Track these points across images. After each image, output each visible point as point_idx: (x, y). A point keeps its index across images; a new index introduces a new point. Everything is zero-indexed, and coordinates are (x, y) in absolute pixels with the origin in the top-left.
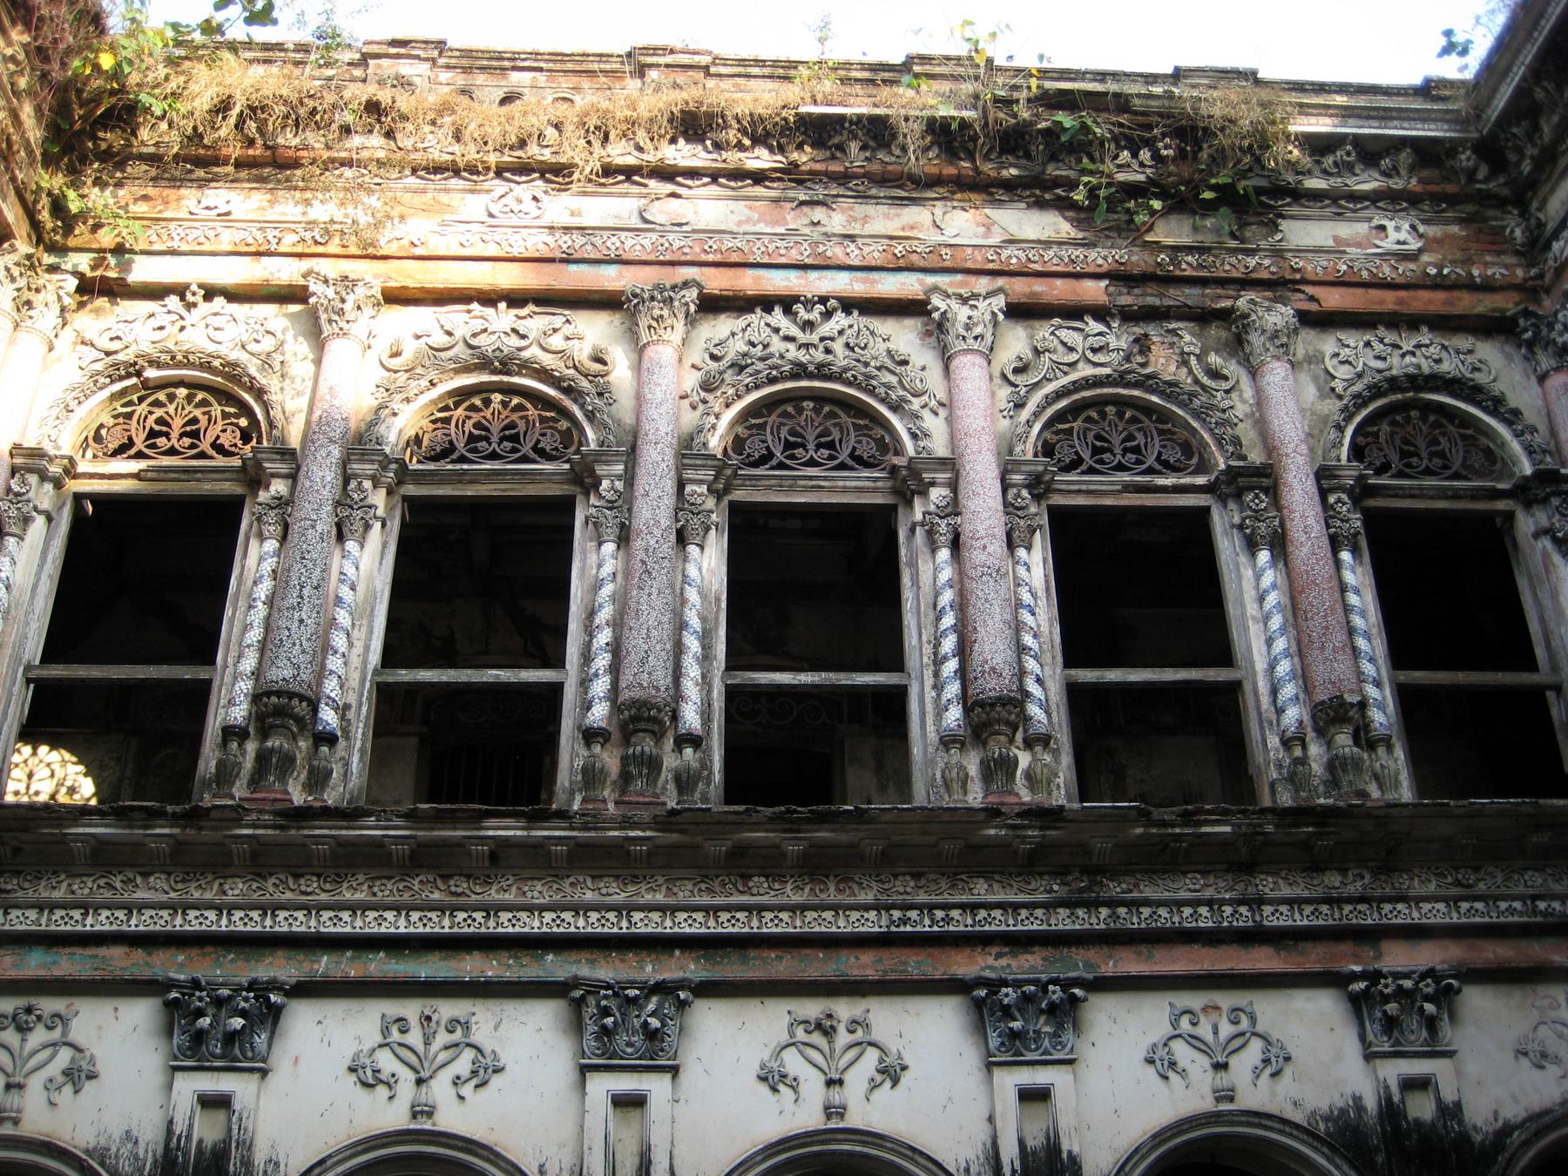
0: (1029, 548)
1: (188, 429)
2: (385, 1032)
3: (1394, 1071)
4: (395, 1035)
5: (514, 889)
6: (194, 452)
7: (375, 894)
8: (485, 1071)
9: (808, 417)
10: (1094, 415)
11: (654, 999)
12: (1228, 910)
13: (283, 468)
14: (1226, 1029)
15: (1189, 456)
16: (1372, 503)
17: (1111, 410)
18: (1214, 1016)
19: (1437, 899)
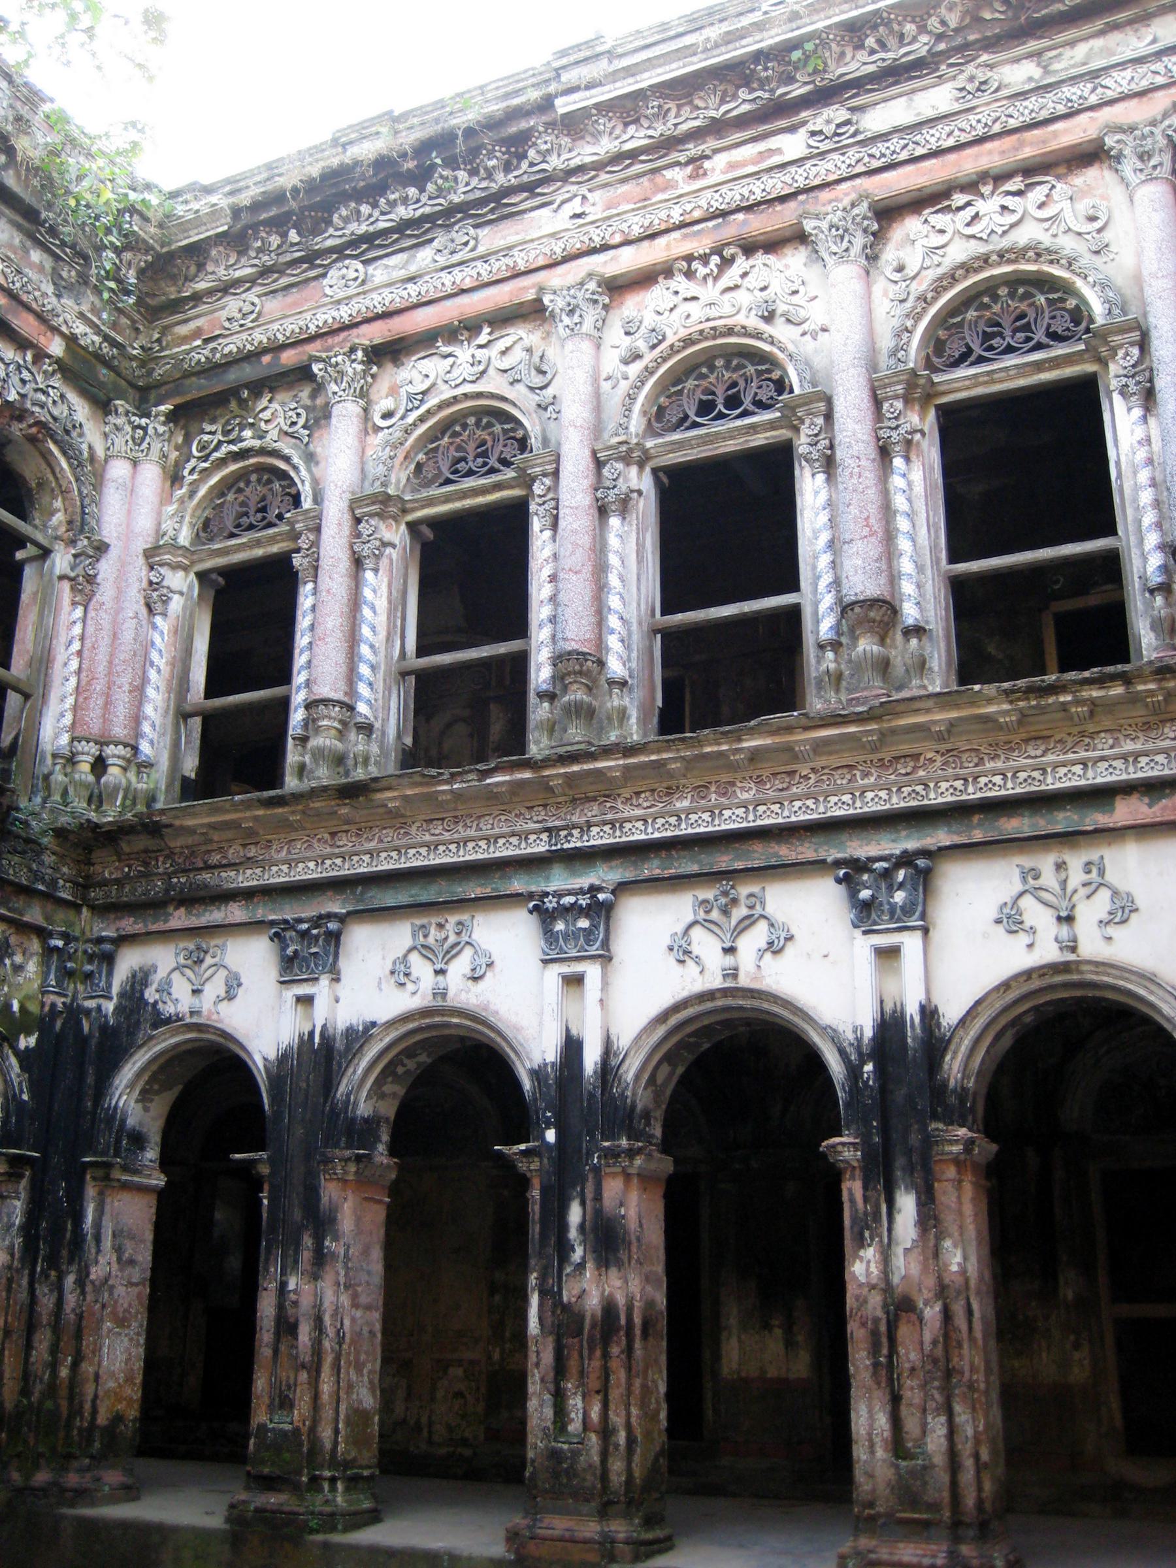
0: (376, 571)
1: (730, 392)
2: (1024, 880)
6: (265, 522)
9: (1005, 306)
15: (1077, 323)
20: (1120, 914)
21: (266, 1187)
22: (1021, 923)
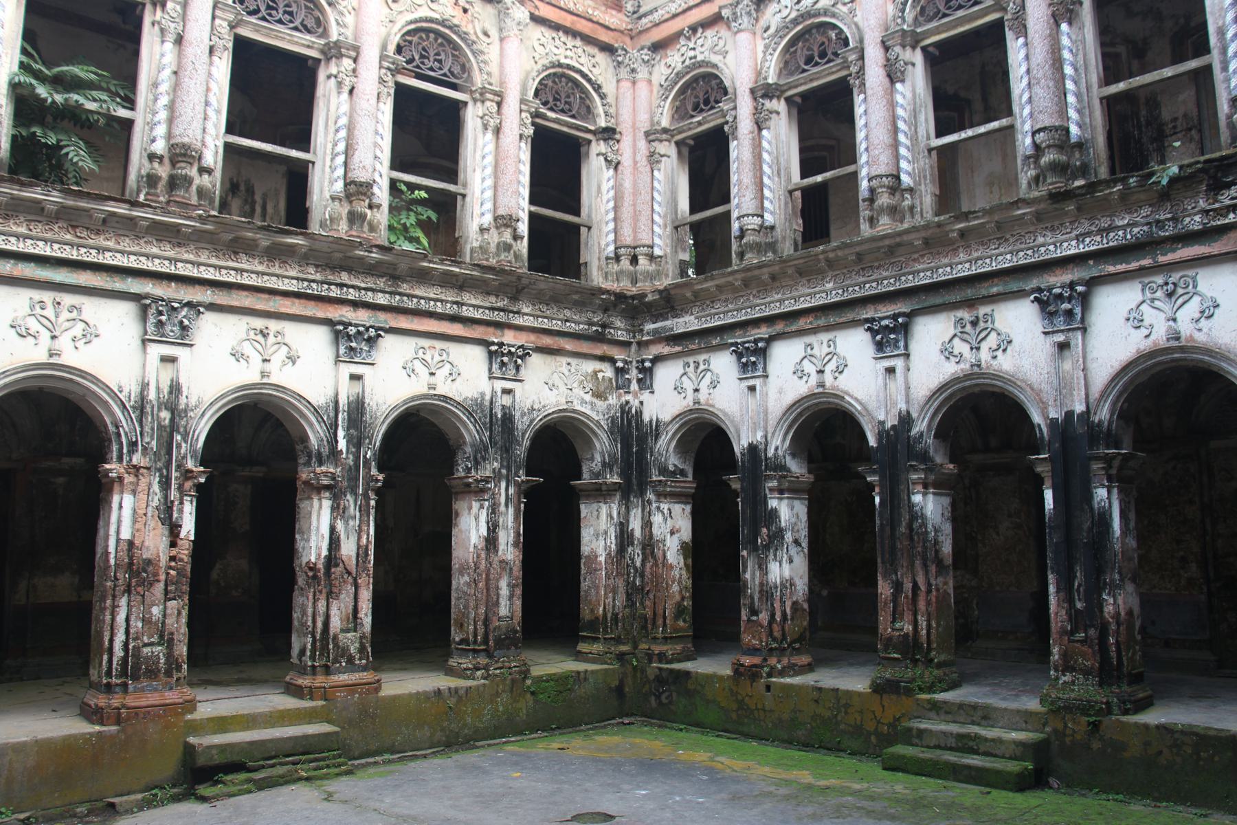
2: (32, 308)
3: (500, 385)
4: (38, 310)
5: (113, 240)
6: (292, 25)
7: (31, 230)
8: (90, 335)
10: (424, 36)
11: (186, 309)
12: (449, 305)
13: (353, 54)
14: (437, 358)
16: (538, 121)
17: (432, 36)
18: (433, 351)
19: (531, 315)
20: (1207, 311)
21: (877, 490)
22: (1142, 321)
